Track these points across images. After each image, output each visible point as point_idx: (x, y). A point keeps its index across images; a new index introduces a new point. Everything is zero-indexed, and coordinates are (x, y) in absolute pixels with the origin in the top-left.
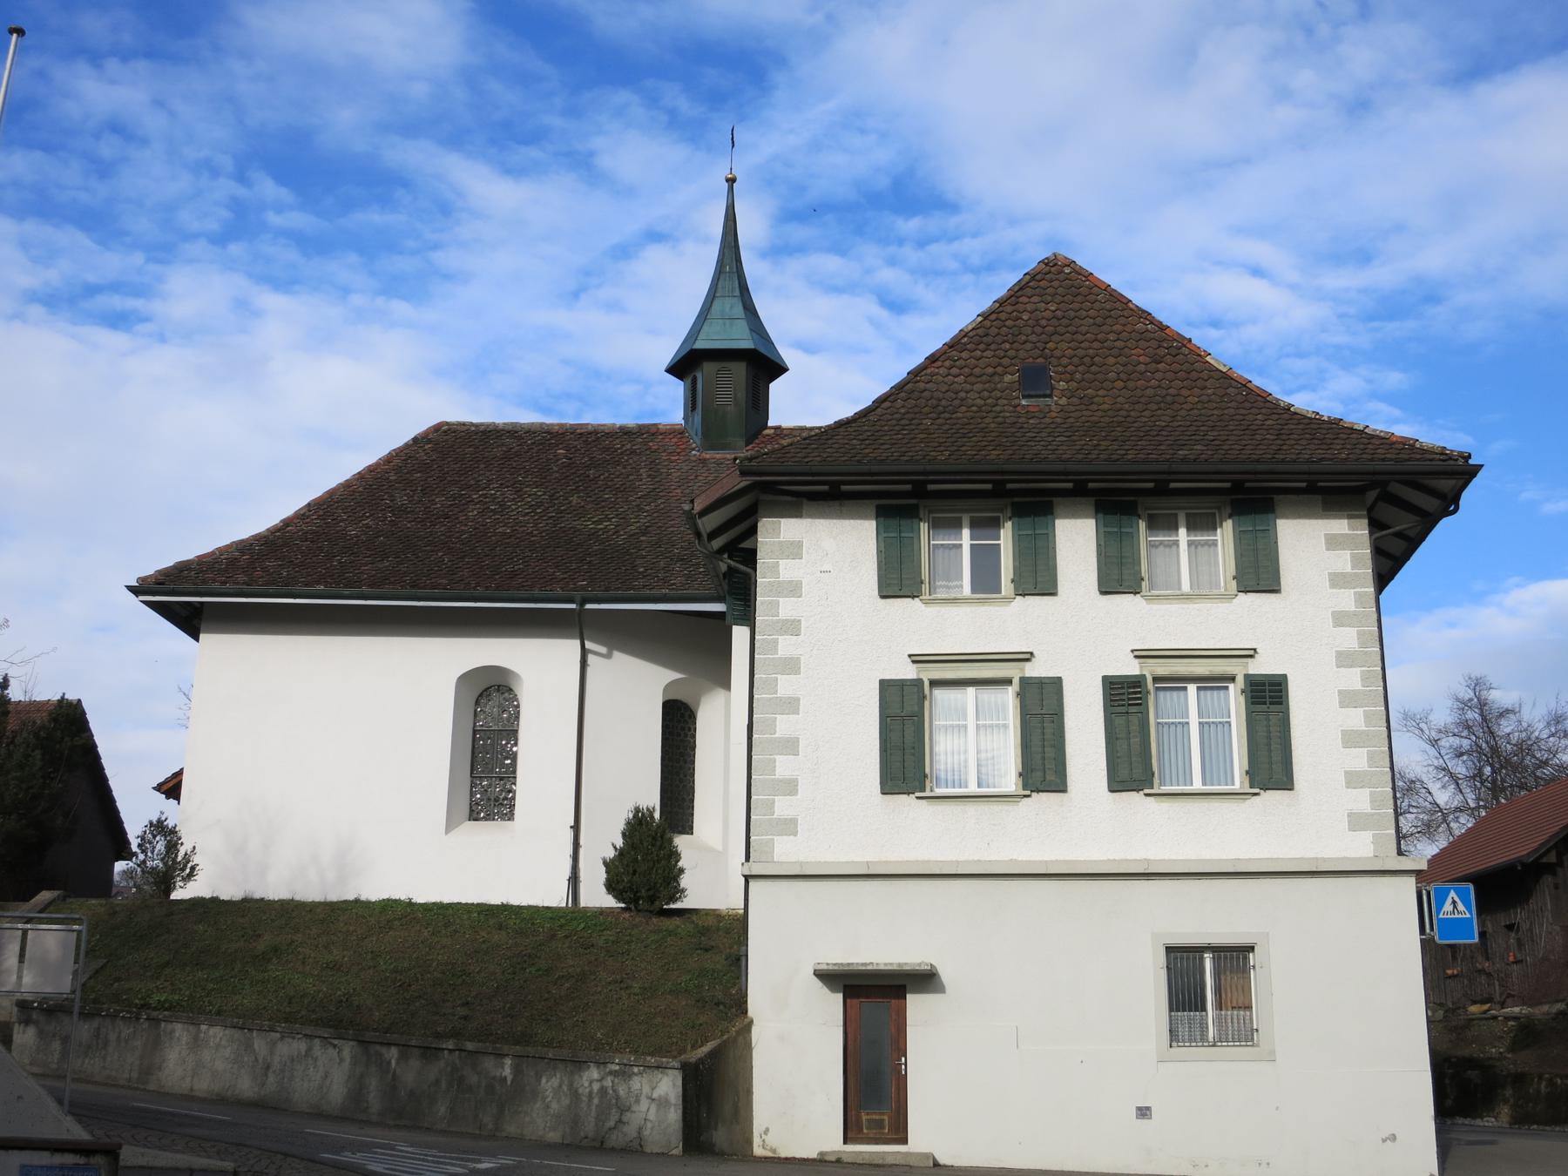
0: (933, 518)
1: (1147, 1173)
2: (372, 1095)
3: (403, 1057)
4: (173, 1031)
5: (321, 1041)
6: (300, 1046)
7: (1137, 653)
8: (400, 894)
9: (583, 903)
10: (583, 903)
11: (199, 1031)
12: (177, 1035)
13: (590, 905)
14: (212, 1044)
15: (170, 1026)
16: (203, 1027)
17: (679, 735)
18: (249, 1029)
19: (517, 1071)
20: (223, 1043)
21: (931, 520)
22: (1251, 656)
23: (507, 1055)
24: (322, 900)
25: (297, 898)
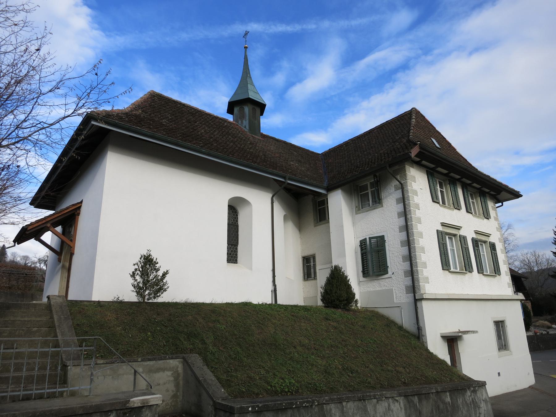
0: (361, 195)
1: (505, 393)
2: (181, 377)
3: (420, 400)
4: (331, 410)
5: (392, 400)
6: (385, 404)
7: (477, 232)
8: (229, 301)
9: (279, 302)
10: (279, 302)
11: (343, 407)
12: (333, 412)
13: (281, 303)
14: (350, 414)
15: (328, 407)
16: (344, 404)
17: (232, 251)
18: (363, 400)
19: (451, 399)
20: (355, 411)
21: (360, 196)
22: (489, 236)
23: (446, 391)
24: (221, 303)
25: (189, 301)
